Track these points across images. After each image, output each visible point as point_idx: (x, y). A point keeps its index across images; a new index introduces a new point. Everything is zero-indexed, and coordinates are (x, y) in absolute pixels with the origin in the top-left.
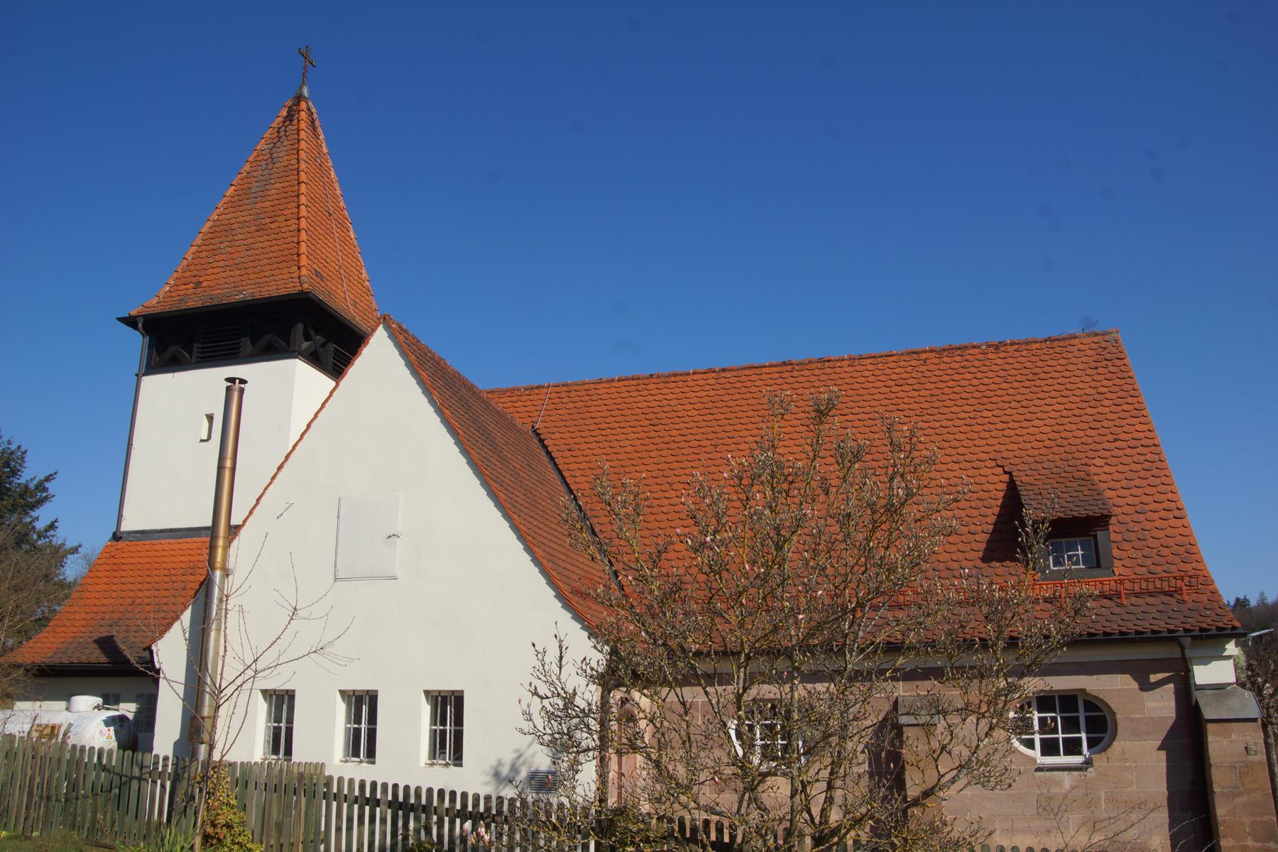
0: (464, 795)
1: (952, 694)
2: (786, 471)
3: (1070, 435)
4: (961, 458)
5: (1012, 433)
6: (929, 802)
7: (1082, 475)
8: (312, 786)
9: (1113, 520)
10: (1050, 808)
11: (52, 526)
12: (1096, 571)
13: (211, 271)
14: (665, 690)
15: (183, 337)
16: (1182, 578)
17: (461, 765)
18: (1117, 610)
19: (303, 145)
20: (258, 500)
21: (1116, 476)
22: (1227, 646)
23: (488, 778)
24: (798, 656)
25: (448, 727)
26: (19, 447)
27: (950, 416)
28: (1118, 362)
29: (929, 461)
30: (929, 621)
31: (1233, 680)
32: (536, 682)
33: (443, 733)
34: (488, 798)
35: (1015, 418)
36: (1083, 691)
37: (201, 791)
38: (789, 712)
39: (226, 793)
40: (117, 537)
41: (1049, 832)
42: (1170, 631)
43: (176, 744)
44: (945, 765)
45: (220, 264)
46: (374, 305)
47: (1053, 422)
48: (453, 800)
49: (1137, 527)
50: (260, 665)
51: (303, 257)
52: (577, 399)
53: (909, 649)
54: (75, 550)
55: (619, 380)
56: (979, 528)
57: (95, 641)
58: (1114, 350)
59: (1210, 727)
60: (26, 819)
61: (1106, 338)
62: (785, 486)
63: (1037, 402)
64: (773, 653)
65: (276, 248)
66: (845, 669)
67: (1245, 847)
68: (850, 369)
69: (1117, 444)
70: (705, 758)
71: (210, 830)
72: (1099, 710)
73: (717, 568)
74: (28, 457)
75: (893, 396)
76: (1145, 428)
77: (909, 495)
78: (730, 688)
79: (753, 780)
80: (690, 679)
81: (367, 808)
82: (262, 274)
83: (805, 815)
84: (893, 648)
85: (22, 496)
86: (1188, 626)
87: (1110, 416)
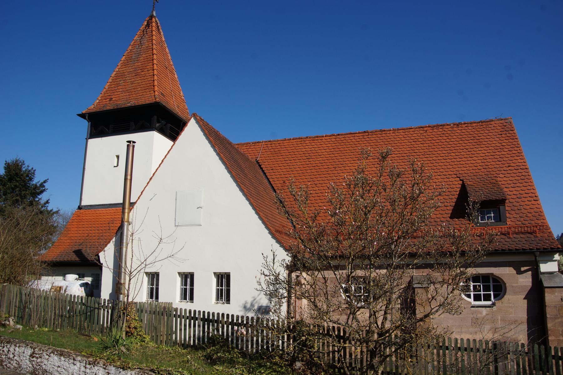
0: (233, 316)
1: (437, 275)
2: (368, 182)
3: (489, 164)
4: (441, 174)
5: (464, 163)
6: (427, 320)
7: (494, 181)
8: (167, 312)
9: (507, 201)
10: (477, 323)
11: (47, 202)
12: (499, 223)
13: (116, 93)
14: (316, 273)
15: (105, 122)
16: (536, 227)
17: (229, 303)
18: (508, 240)
19: (154, 37)
20: (142, 193)
21: (509, 182)
22: (555, 256)
23: (241, 309)
24: (373, 260)
25: (188, 287)
26: (32, 168)
27: (437, 155)
28: (511, 132)
29: (430, 178)
30: (428, 245)
31: (557, 270)
32: (263, 269)
33: (222, 290)
34: (242, 317)
35: (465, 156)
36: (492, 274)
37: (124, 313)
38: (369, 282)
39: (134, 315)
40: (80, 208)
41: (476, 333)
42: (530, 249)
43: (110, 295)
44: (434, 304)
45: (120, 90)
46: (186, 107)
47: (482, 158)
48: (228, 317)
49: (517, 204)
50: (148, 262)
51: (156, 87)
52: (275, 147)
53: (419, 256)
54: (57, 212)
55: (293, 139)
56: (449, 204)
57: (73, 252)
58: (510, 127)
59: (546, 290)
60: (54, 324)
61: (506, 121)
62: (368, 188)
63: (475, 149)
64: (363, 257)
65: (144, 83)
66: (392, 264)
67: (559, 340)
68: (394, 134)
69: (510, 168)
70: (335, 301)
71: (128, 330)
72: (500, 282)
73: (342, 223)
74: (36, 173)
75: (412, 146)
76: (522, 161)
77: (421, 193)
78: (344, 271)
79: (354, 310)
80: (328, 267)
81: (192, 321)
82: (138, 95)
83: (375, 325)
84: (413, 255)
85: (34, 189)
86: (538, 247)
87: (507, 156)
